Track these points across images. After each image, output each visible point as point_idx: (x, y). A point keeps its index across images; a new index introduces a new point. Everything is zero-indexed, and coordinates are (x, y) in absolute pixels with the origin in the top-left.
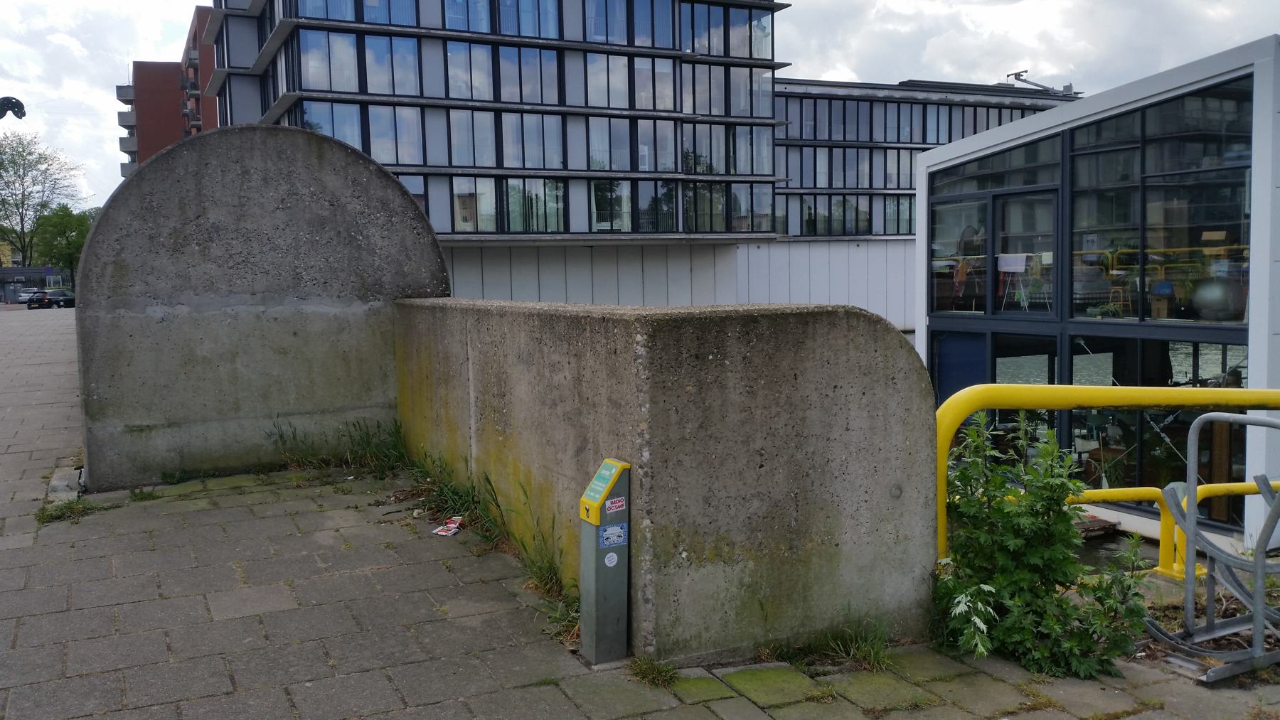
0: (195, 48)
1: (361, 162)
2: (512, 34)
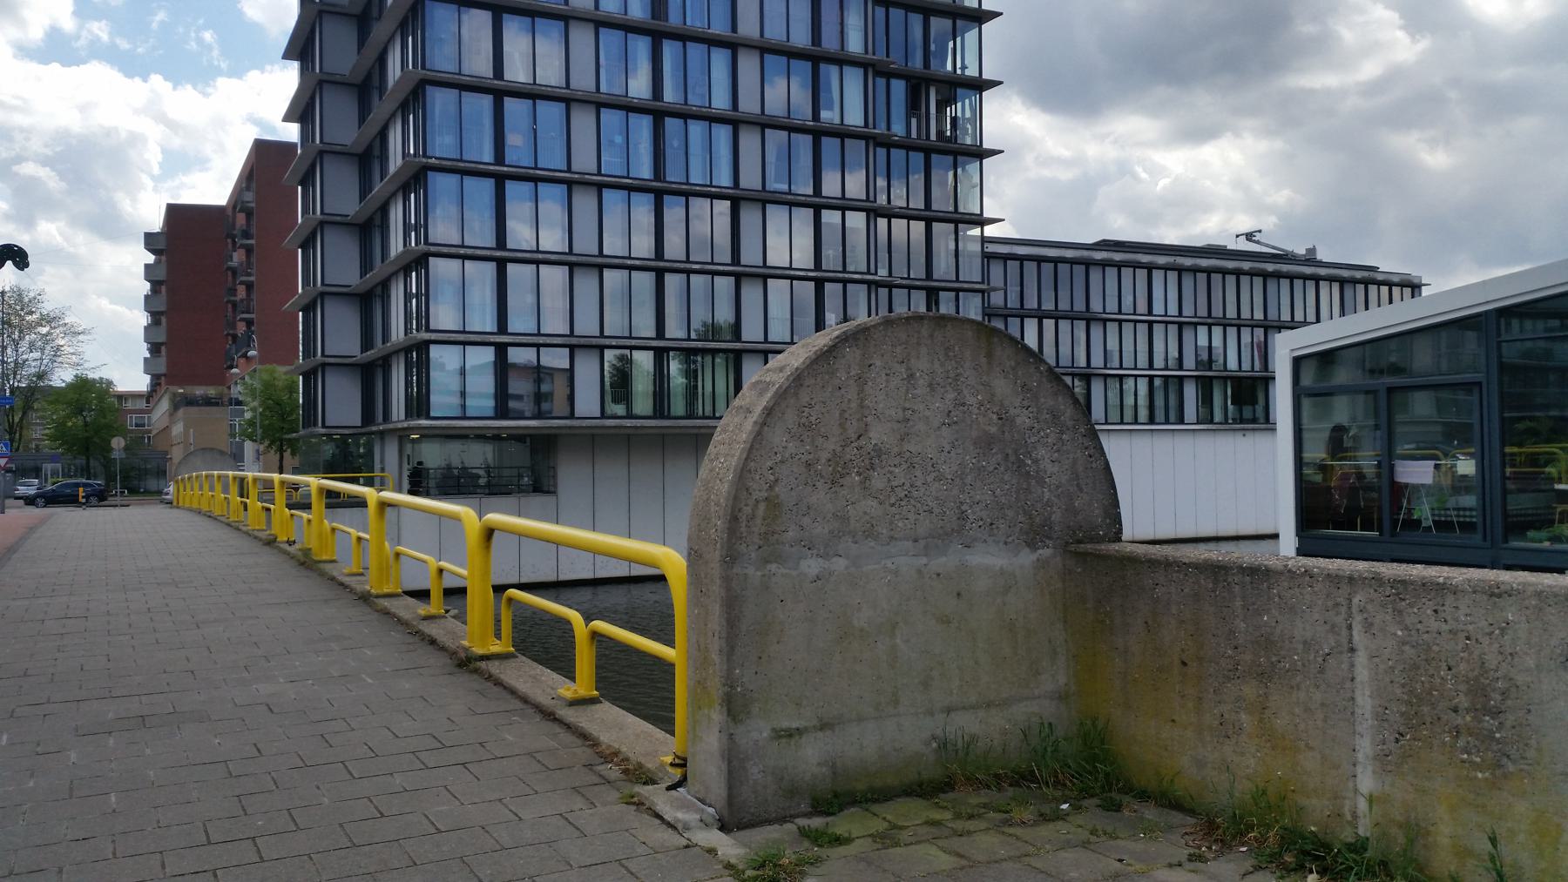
0: (248, 188)
2: (678, 181)
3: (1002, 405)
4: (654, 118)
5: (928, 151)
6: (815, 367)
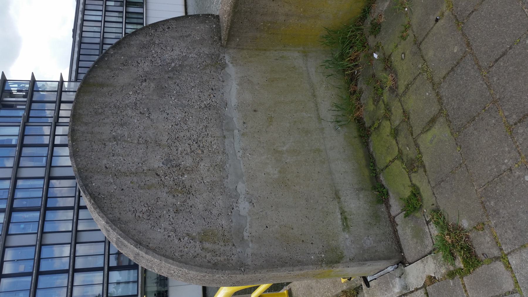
1: (106, 59)
2: (41, 201)
3: (136, 79)
4: (13, 212)
5: (31, 102)
6: (106, 209)
